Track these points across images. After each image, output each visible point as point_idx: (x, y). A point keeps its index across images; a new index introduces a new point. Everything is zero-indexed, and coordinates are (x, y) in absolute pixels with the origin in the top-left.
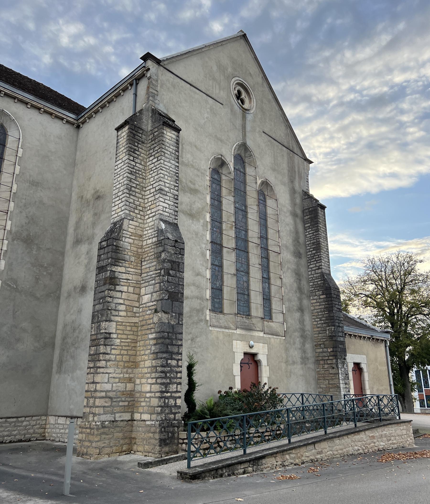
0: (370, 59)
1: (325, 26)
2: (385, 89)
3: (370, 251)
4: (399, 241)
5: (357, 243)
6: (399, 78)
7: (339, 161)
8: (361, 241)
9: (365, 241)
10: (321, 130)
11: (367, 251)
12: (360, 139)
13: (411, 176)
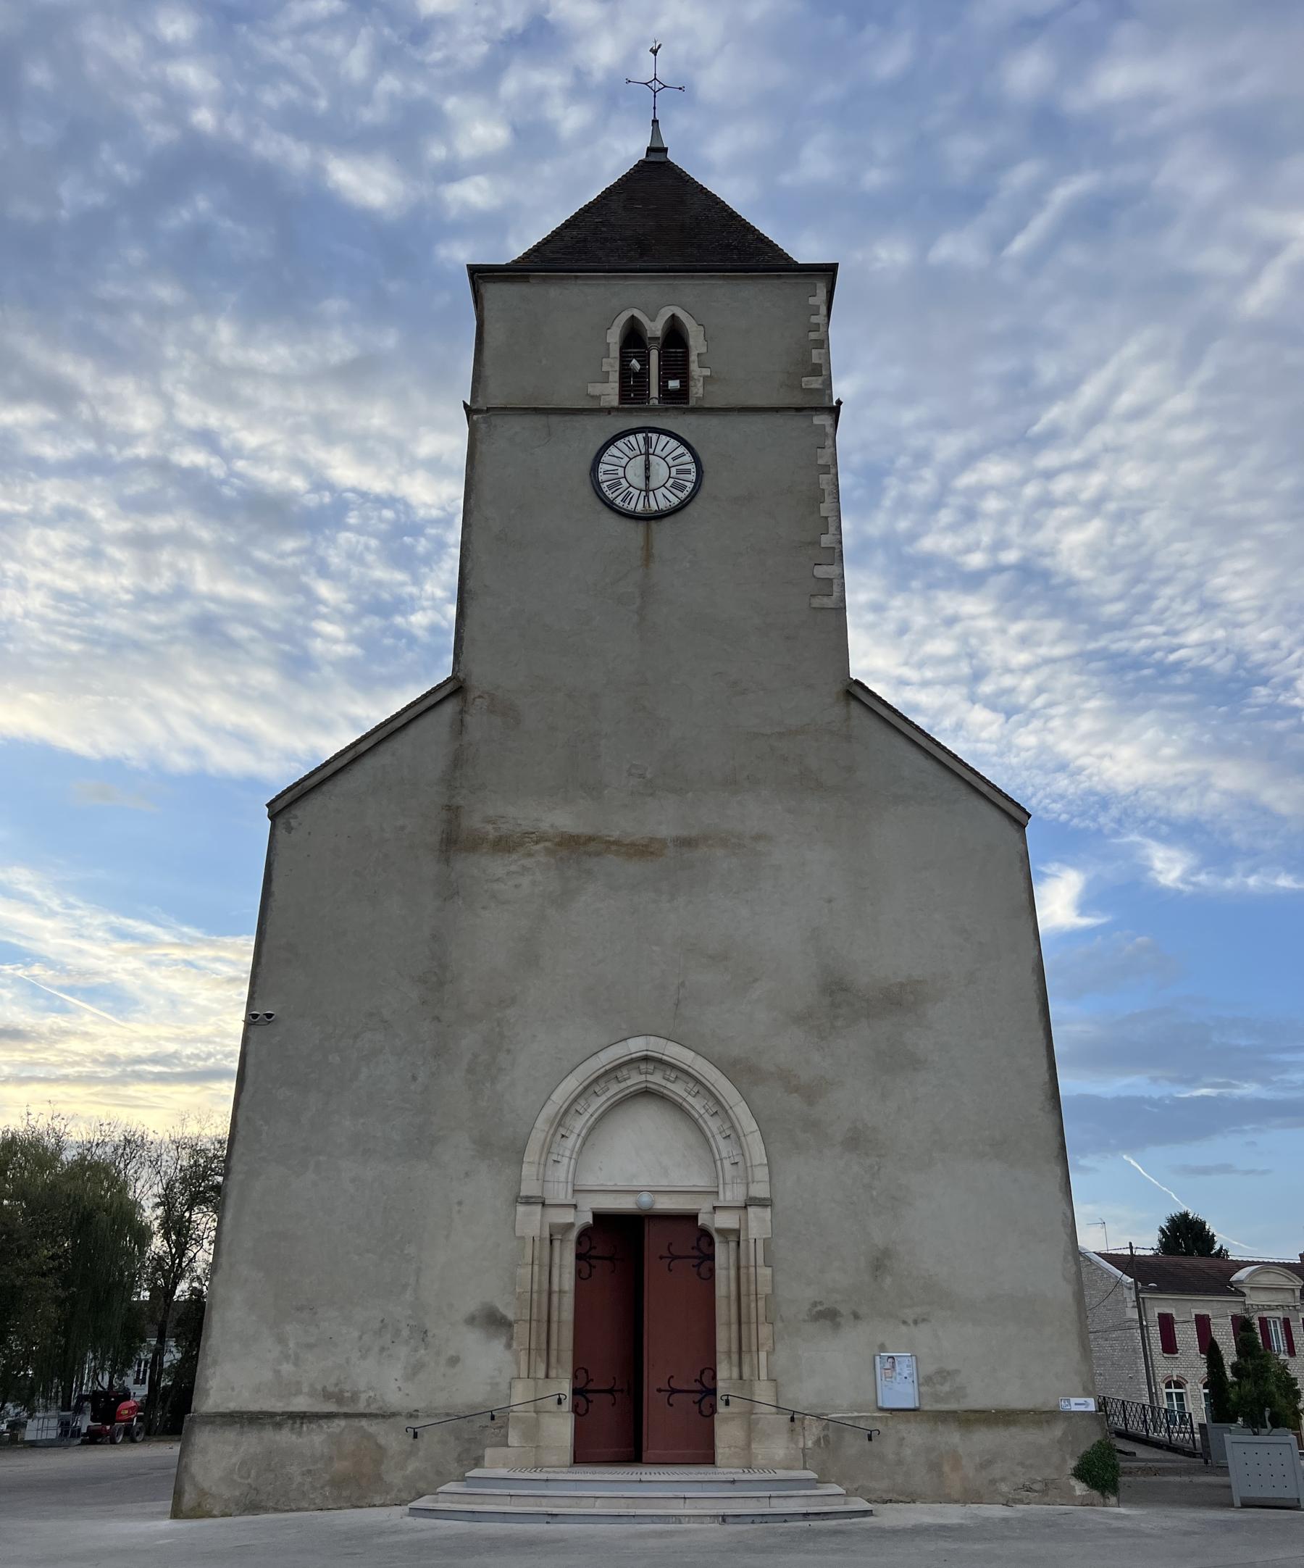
0: (284, 380)
1: (186, 214)
2: (298, 483)
3: (90, 938)
4: (185, 929)
5: (55, 904)
6: (345, 471)
7: (95, 638)
8: (71, 900)
9: (81, 904)
10: (63, 516)
11: (81, 936)
12: (180, 593)
13: (290, 756)
